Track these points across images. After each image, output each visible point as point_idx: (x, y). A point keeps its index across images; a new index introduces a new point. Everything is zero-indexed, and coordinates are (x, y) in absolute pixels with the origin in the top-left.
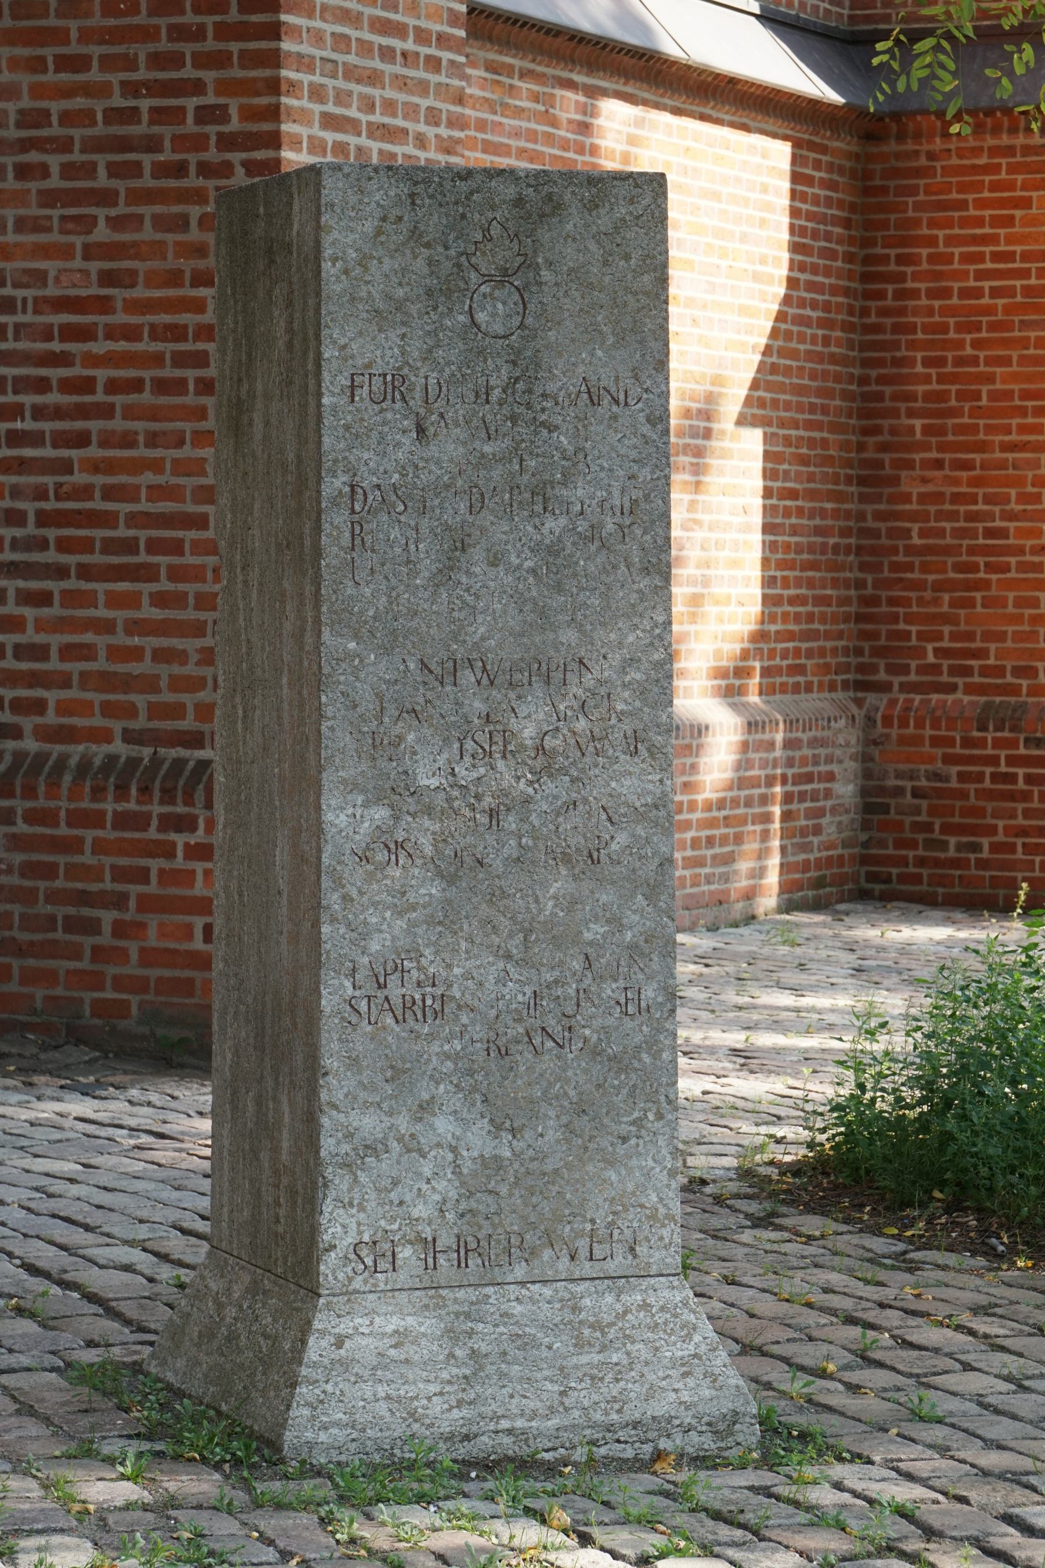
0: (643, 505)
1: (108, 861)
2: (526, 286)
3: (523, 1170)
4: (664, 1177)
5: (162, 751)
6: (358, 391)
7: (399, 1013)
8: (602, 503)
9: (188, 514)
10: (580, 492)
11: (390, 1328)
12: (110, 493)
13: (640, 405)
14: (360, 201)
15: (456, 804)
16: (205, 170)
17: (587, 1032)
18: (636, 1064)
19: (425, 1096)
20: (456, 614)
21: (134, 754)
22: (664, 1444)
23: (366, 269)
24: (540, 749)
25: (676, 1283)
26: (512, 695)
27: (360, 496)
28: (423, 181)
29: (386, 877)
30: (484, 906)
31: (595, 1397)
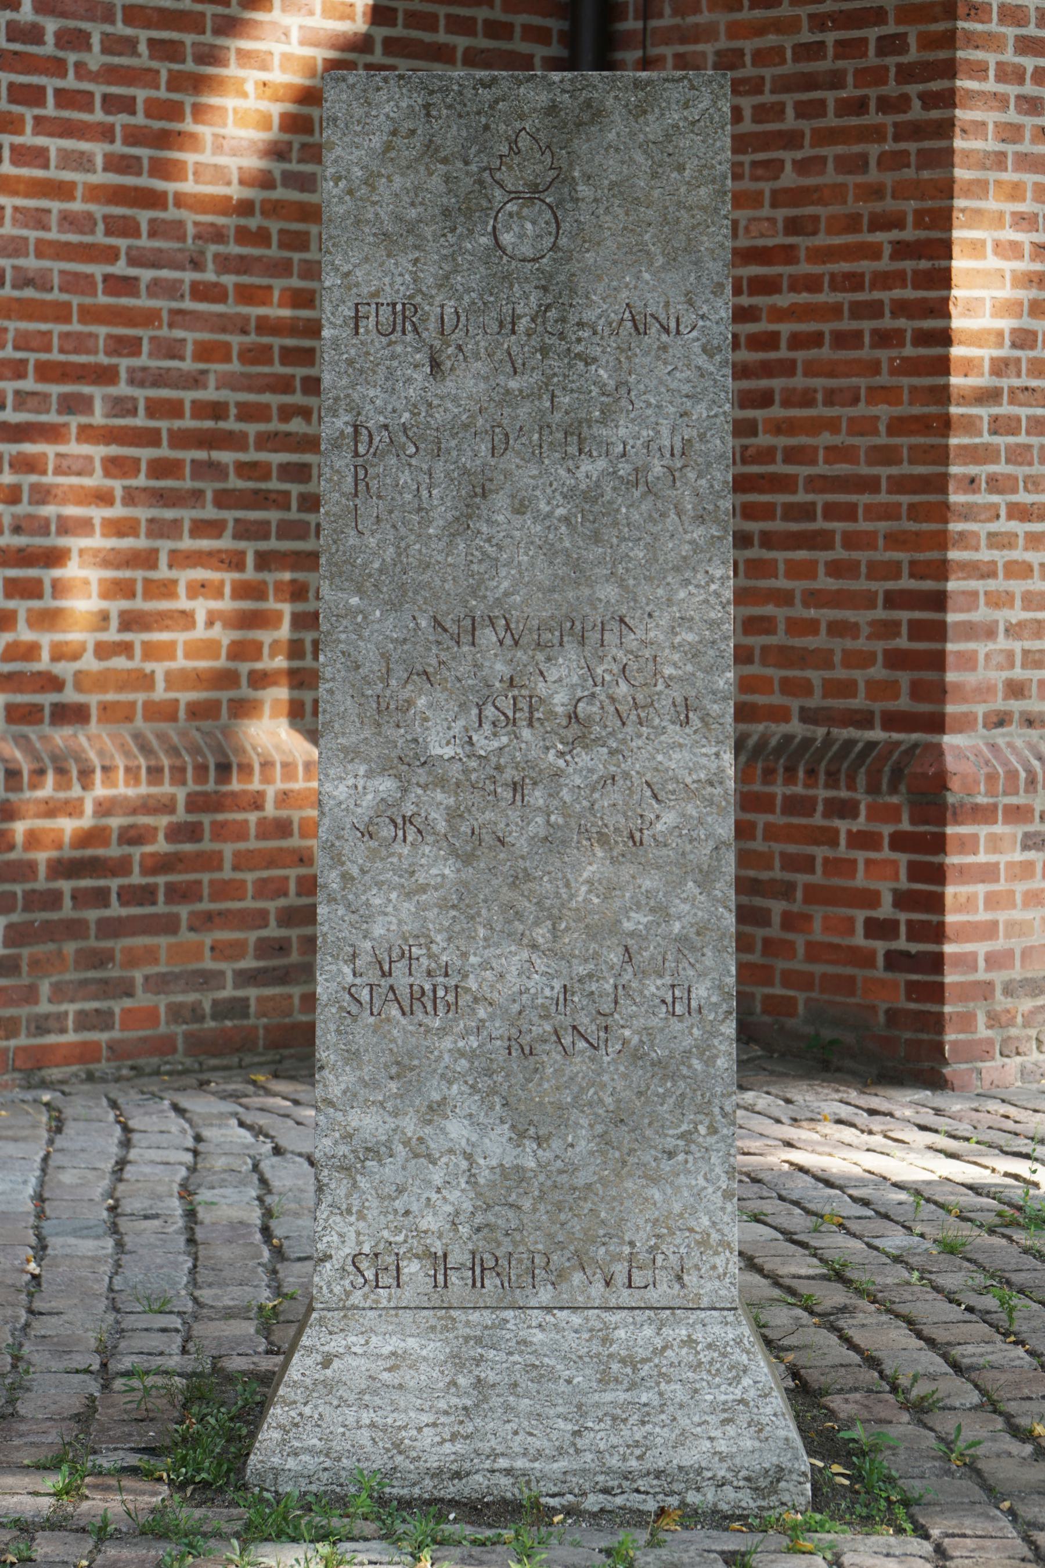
0: (697, 446)
1: (777, 847)
2: (560, 203)
3: (549, 1183)
4: (718, 1199)
5: (835, 731)
6: (362, 323)
7: (406, 1004)
8: (647, 445)
9: (860, 477)
10: (622, 432)
11: (386, 1350)
12: (792, 455)
13: (694, 334)
14: (367, 115)
15: (474, 776)
16: (885, 105)
17: (627, 1033)
18: (685, 1071)
19: (436, 1096)
20: (475, 567)
21: (809, 734)
22: (692, 1497)
23: (373, 188)
24: (573, 717)
25: (731, 1319)
26: (540, 657)
28: (440, 90)
29: (392, 855)
30: (505, 889)
31: (614, 1440)
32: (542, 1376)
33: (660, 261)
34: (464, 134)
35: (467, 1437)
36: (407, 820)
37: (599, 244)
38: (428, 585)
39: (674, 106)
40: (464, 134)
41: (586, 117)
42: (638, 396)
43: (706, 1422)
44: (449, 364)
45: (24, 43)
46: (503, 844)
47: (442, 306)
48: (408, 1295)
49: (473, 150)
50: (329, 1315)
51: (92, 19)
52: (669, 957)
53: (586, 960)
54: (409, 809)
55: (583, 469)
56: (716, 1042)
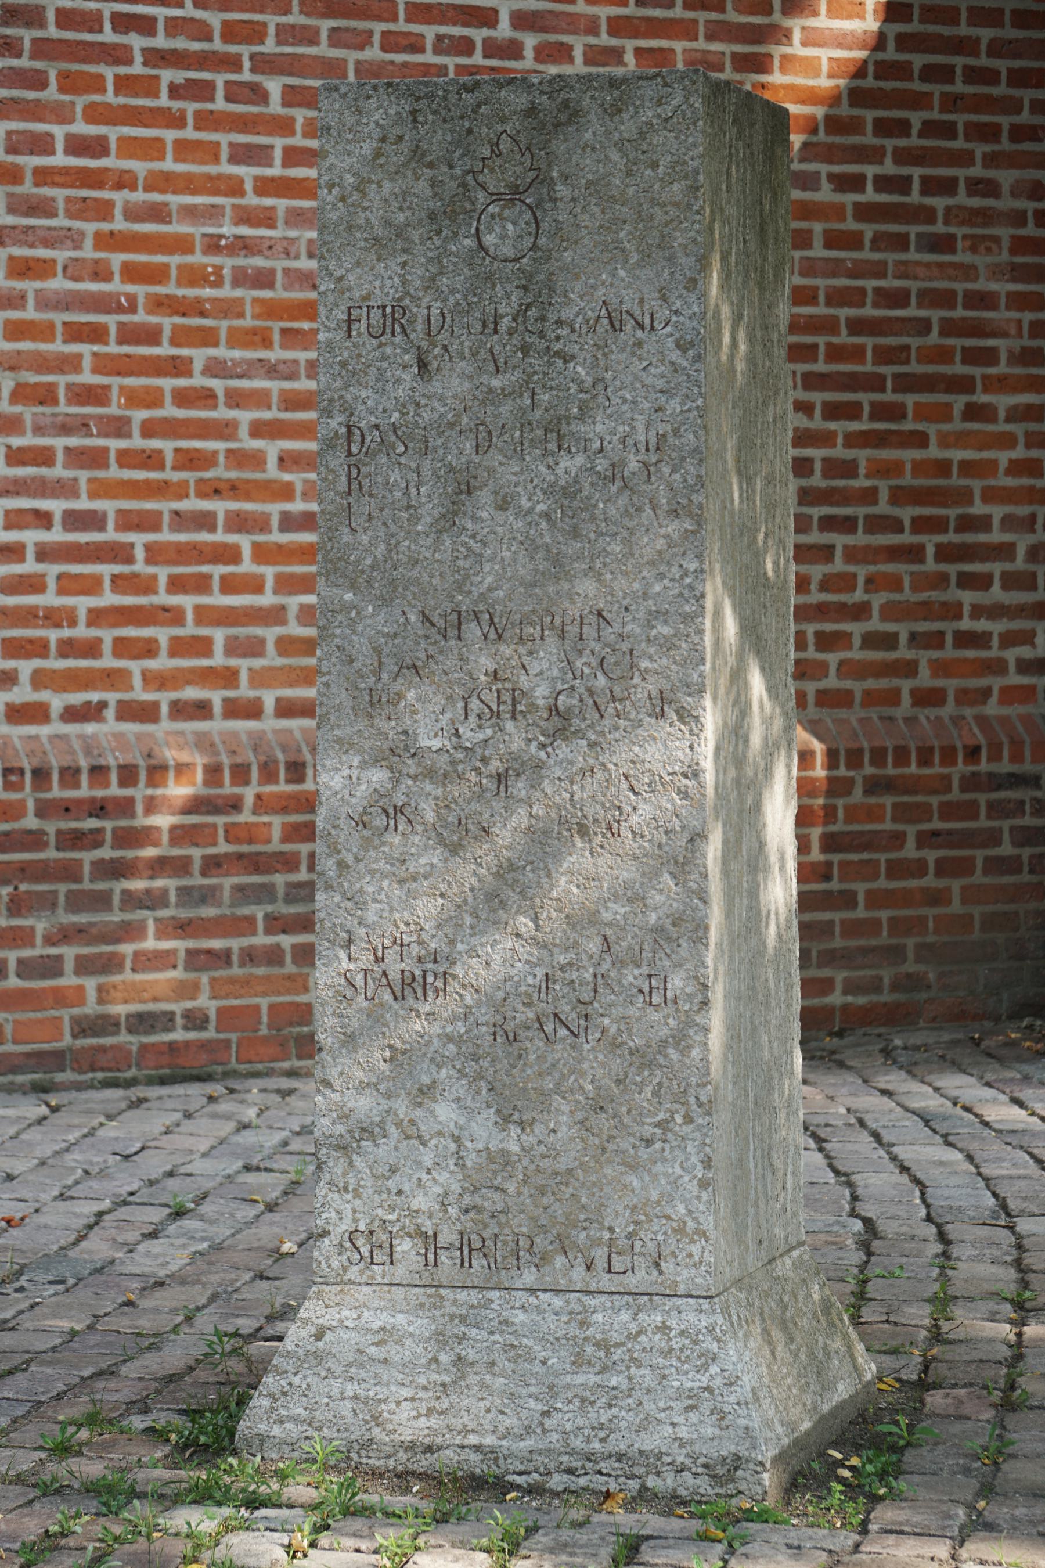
0: (671, 440)
2: (539, 203)
3: (533, 1167)
4: (693, 1188)
7: (398, 989)
10: (599, 428)
11: (376, 1325)
13: (668, 329)
15: (460, 768)
17: (606, 1021)
18: (661, 1060)
19: (426, 1080)
20: (461, 563)
22: (651, 1482)
23: (364, 194)
24: (554, 709)
26: (522, 650)
27: (357, 437)
28: (426, 96)
29: (384, 844)
31: (581, 1422)
32: (519, 1356)
33: (635, 258)
34: (449, 138)
35: (441, 1413)
36: (399, 810)
37: (576, 243)
38: (417, 581)
39: (648, 104)
40: (449, 138)
41: (563, 118)
42: (614, 392)
43: (670, 1408)
44: (435, 364)
45: (501, 58)
46: (488, 834)
47: (429, 308)
48: (400, 1272)
49: (457, 154)
50: (327, 1288)
51: (575, 33)
52: (646, 947)
53: (567, 949)
54: (399, 799)
55: (562, 465)
56: (691, 1032)
